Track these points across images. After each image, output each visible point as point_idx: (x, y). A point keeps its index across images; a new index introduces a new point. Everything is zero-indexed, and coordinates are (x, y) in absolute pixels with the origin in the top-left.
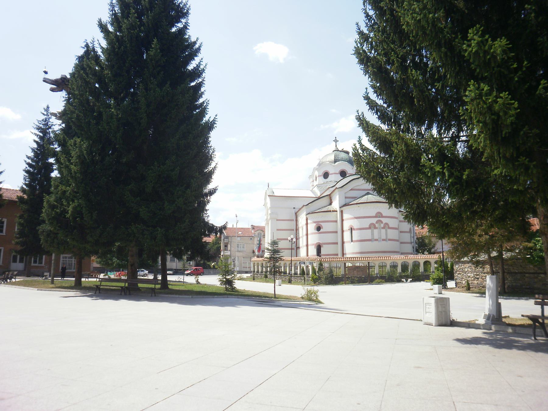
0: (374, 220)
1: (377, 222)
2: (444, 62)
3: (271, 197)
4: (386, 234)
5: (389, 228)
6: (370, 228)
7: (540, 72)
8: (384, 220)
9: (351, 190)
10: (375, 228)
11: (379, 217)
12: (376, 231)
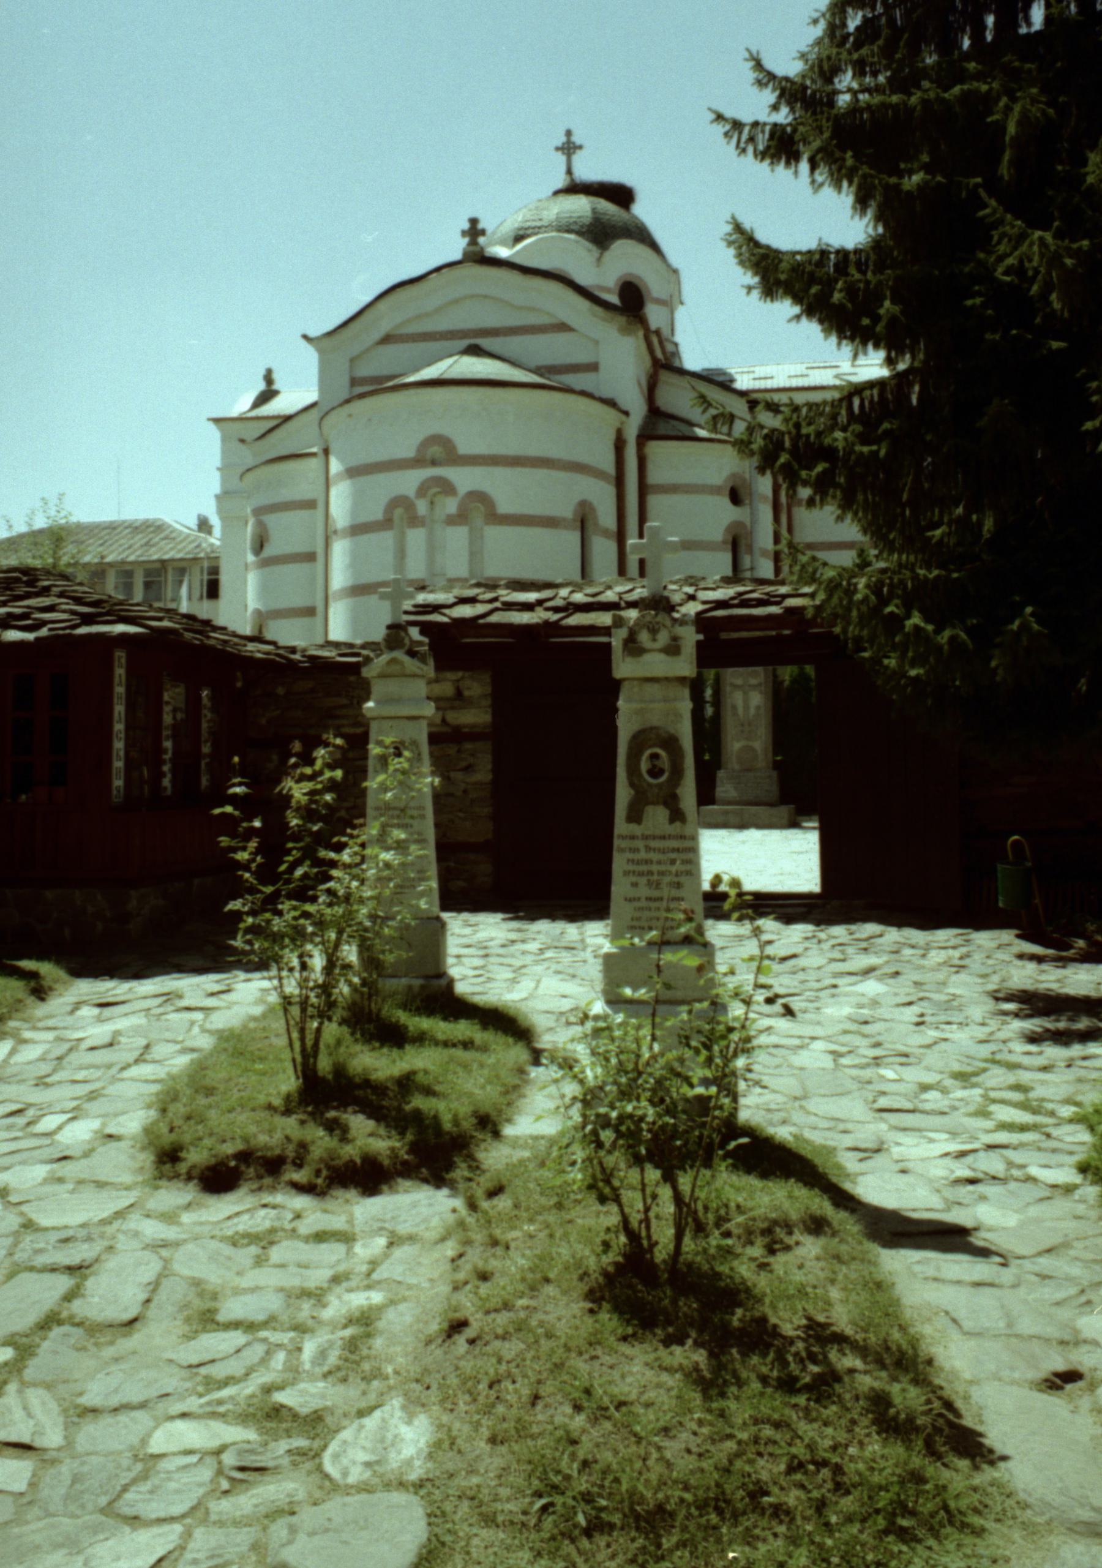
0: (409, 482)
1: (422, 491)
2: (1004, 100)
3: (223, 424)
4: (401, 553)
5: (496, 518)
6: (386, 523)
7: (886, 78)
8: (465, 479)
9: (387, 339)
10: (414, 521)
11: (434, 463)
12: (416, 538)
